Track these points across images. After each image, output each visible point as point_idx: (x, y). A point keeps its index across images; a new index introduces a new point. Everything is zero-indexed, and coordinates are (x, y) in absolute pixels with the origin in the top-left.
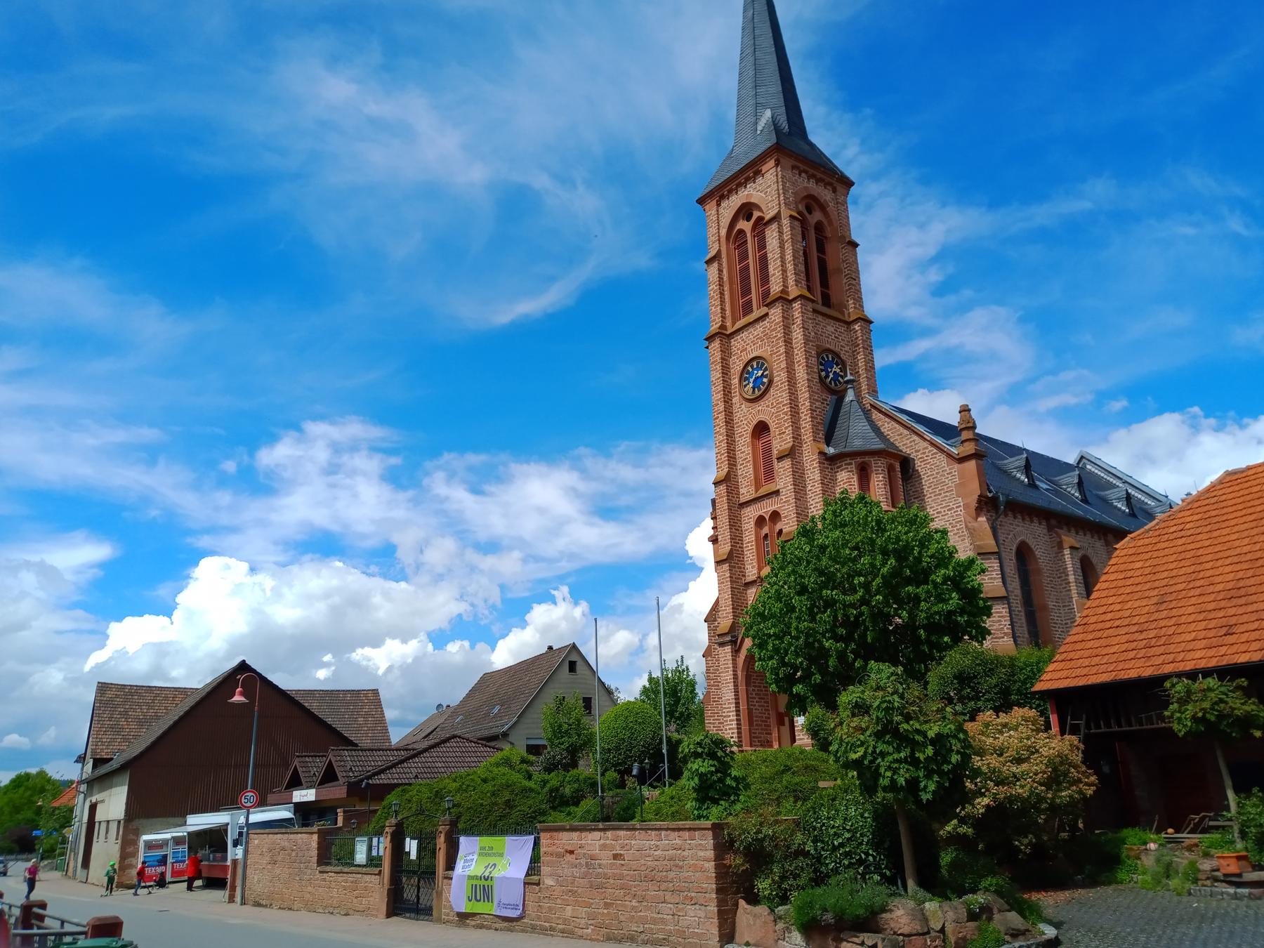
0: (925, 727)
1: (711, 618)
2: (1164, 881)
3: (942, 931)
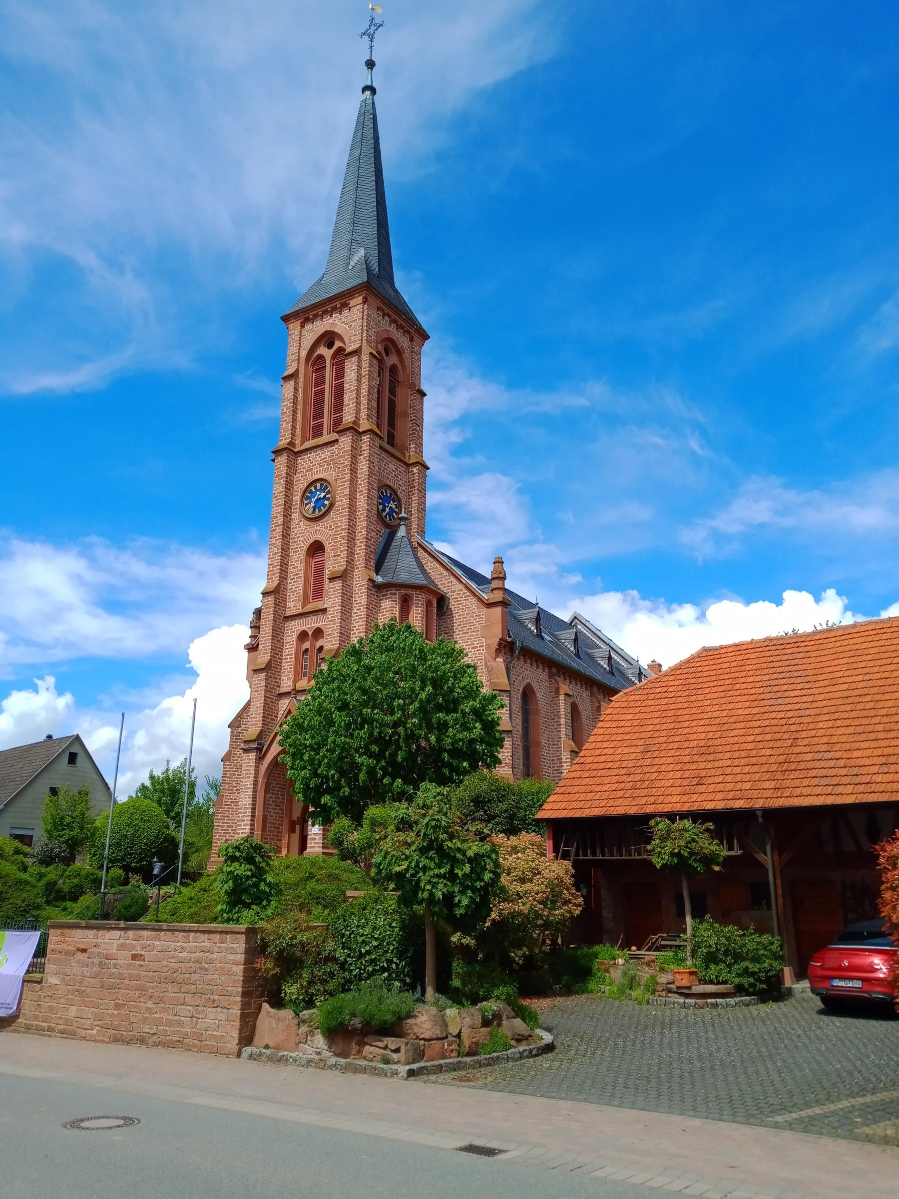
0: (465, 846)
1: (235, 724)
2: (628, 991)
3: (459, 1036)
